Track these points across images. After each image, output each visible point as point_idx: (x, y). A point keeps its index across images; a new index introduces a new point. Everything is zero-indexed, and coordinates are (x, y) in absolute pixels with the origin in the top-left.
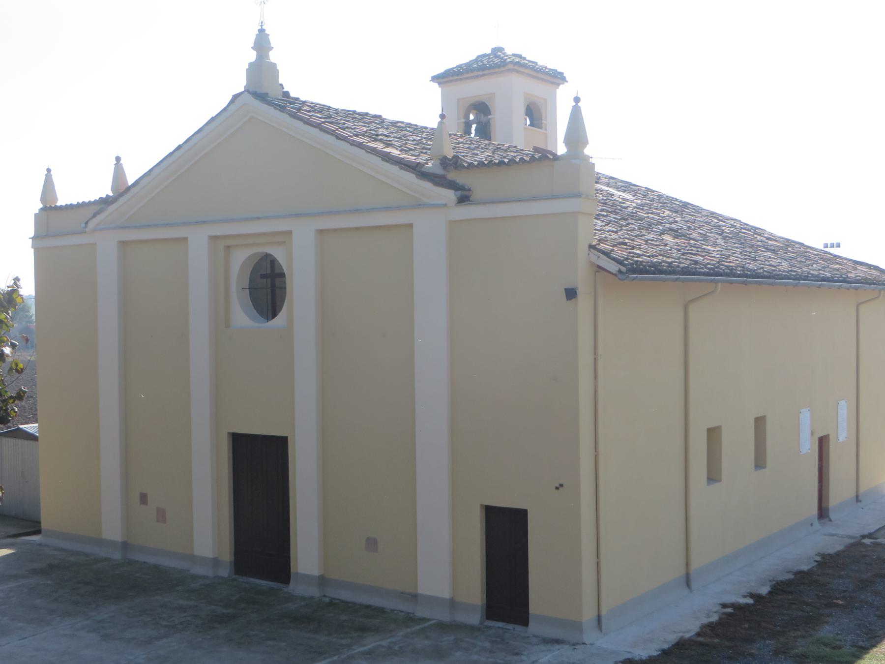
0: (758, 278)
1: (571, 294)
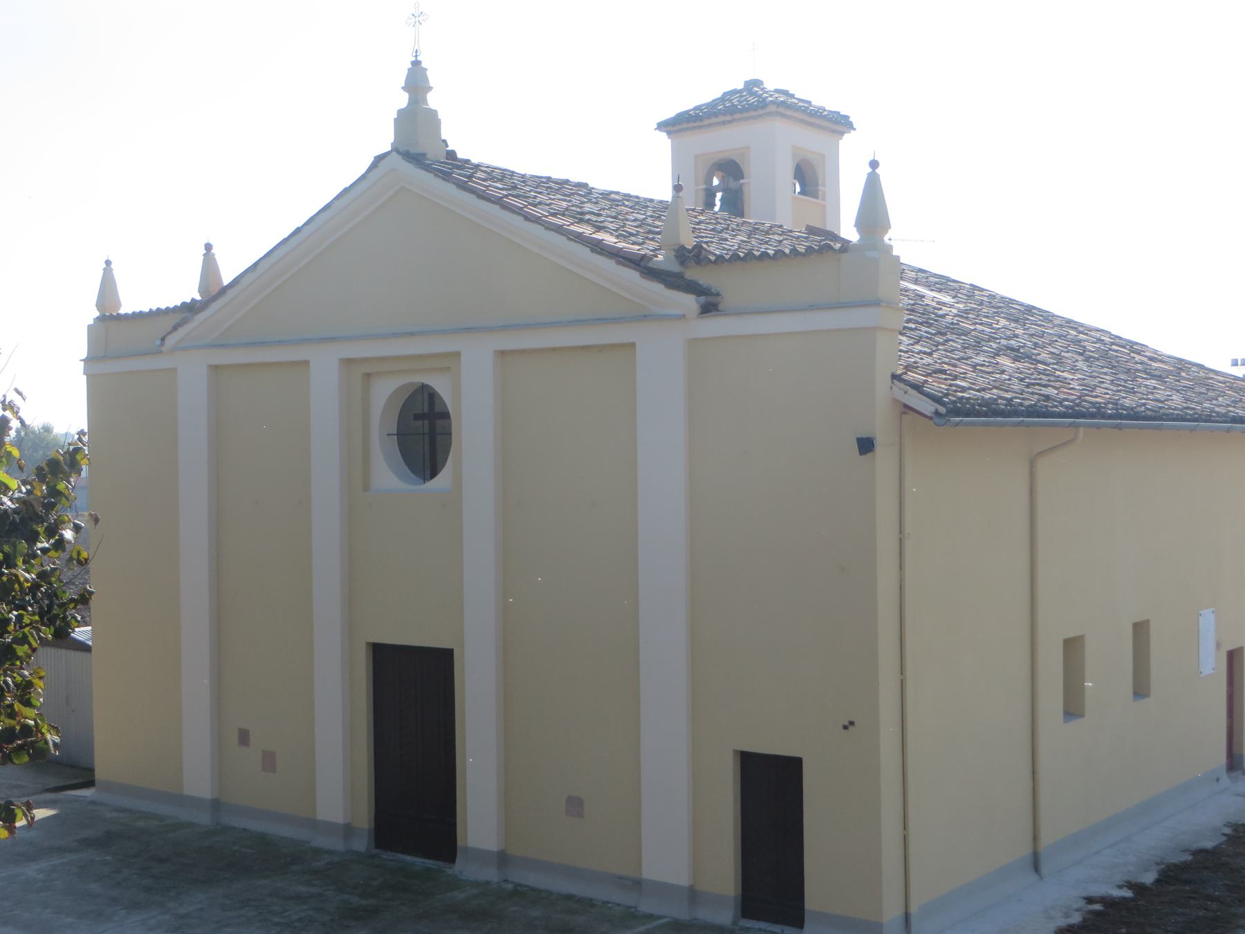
0: (1138, 419)
1: (866, 445)
